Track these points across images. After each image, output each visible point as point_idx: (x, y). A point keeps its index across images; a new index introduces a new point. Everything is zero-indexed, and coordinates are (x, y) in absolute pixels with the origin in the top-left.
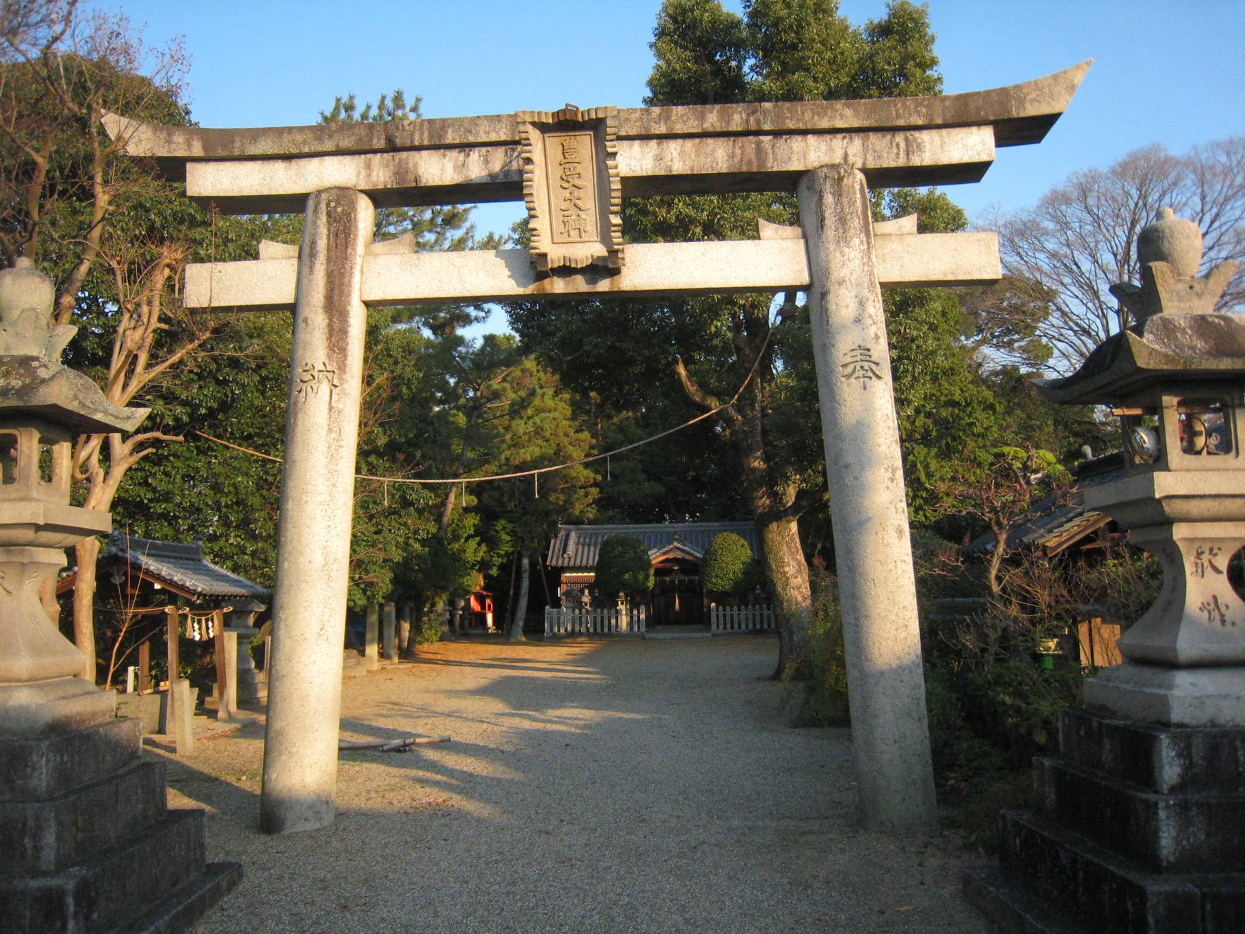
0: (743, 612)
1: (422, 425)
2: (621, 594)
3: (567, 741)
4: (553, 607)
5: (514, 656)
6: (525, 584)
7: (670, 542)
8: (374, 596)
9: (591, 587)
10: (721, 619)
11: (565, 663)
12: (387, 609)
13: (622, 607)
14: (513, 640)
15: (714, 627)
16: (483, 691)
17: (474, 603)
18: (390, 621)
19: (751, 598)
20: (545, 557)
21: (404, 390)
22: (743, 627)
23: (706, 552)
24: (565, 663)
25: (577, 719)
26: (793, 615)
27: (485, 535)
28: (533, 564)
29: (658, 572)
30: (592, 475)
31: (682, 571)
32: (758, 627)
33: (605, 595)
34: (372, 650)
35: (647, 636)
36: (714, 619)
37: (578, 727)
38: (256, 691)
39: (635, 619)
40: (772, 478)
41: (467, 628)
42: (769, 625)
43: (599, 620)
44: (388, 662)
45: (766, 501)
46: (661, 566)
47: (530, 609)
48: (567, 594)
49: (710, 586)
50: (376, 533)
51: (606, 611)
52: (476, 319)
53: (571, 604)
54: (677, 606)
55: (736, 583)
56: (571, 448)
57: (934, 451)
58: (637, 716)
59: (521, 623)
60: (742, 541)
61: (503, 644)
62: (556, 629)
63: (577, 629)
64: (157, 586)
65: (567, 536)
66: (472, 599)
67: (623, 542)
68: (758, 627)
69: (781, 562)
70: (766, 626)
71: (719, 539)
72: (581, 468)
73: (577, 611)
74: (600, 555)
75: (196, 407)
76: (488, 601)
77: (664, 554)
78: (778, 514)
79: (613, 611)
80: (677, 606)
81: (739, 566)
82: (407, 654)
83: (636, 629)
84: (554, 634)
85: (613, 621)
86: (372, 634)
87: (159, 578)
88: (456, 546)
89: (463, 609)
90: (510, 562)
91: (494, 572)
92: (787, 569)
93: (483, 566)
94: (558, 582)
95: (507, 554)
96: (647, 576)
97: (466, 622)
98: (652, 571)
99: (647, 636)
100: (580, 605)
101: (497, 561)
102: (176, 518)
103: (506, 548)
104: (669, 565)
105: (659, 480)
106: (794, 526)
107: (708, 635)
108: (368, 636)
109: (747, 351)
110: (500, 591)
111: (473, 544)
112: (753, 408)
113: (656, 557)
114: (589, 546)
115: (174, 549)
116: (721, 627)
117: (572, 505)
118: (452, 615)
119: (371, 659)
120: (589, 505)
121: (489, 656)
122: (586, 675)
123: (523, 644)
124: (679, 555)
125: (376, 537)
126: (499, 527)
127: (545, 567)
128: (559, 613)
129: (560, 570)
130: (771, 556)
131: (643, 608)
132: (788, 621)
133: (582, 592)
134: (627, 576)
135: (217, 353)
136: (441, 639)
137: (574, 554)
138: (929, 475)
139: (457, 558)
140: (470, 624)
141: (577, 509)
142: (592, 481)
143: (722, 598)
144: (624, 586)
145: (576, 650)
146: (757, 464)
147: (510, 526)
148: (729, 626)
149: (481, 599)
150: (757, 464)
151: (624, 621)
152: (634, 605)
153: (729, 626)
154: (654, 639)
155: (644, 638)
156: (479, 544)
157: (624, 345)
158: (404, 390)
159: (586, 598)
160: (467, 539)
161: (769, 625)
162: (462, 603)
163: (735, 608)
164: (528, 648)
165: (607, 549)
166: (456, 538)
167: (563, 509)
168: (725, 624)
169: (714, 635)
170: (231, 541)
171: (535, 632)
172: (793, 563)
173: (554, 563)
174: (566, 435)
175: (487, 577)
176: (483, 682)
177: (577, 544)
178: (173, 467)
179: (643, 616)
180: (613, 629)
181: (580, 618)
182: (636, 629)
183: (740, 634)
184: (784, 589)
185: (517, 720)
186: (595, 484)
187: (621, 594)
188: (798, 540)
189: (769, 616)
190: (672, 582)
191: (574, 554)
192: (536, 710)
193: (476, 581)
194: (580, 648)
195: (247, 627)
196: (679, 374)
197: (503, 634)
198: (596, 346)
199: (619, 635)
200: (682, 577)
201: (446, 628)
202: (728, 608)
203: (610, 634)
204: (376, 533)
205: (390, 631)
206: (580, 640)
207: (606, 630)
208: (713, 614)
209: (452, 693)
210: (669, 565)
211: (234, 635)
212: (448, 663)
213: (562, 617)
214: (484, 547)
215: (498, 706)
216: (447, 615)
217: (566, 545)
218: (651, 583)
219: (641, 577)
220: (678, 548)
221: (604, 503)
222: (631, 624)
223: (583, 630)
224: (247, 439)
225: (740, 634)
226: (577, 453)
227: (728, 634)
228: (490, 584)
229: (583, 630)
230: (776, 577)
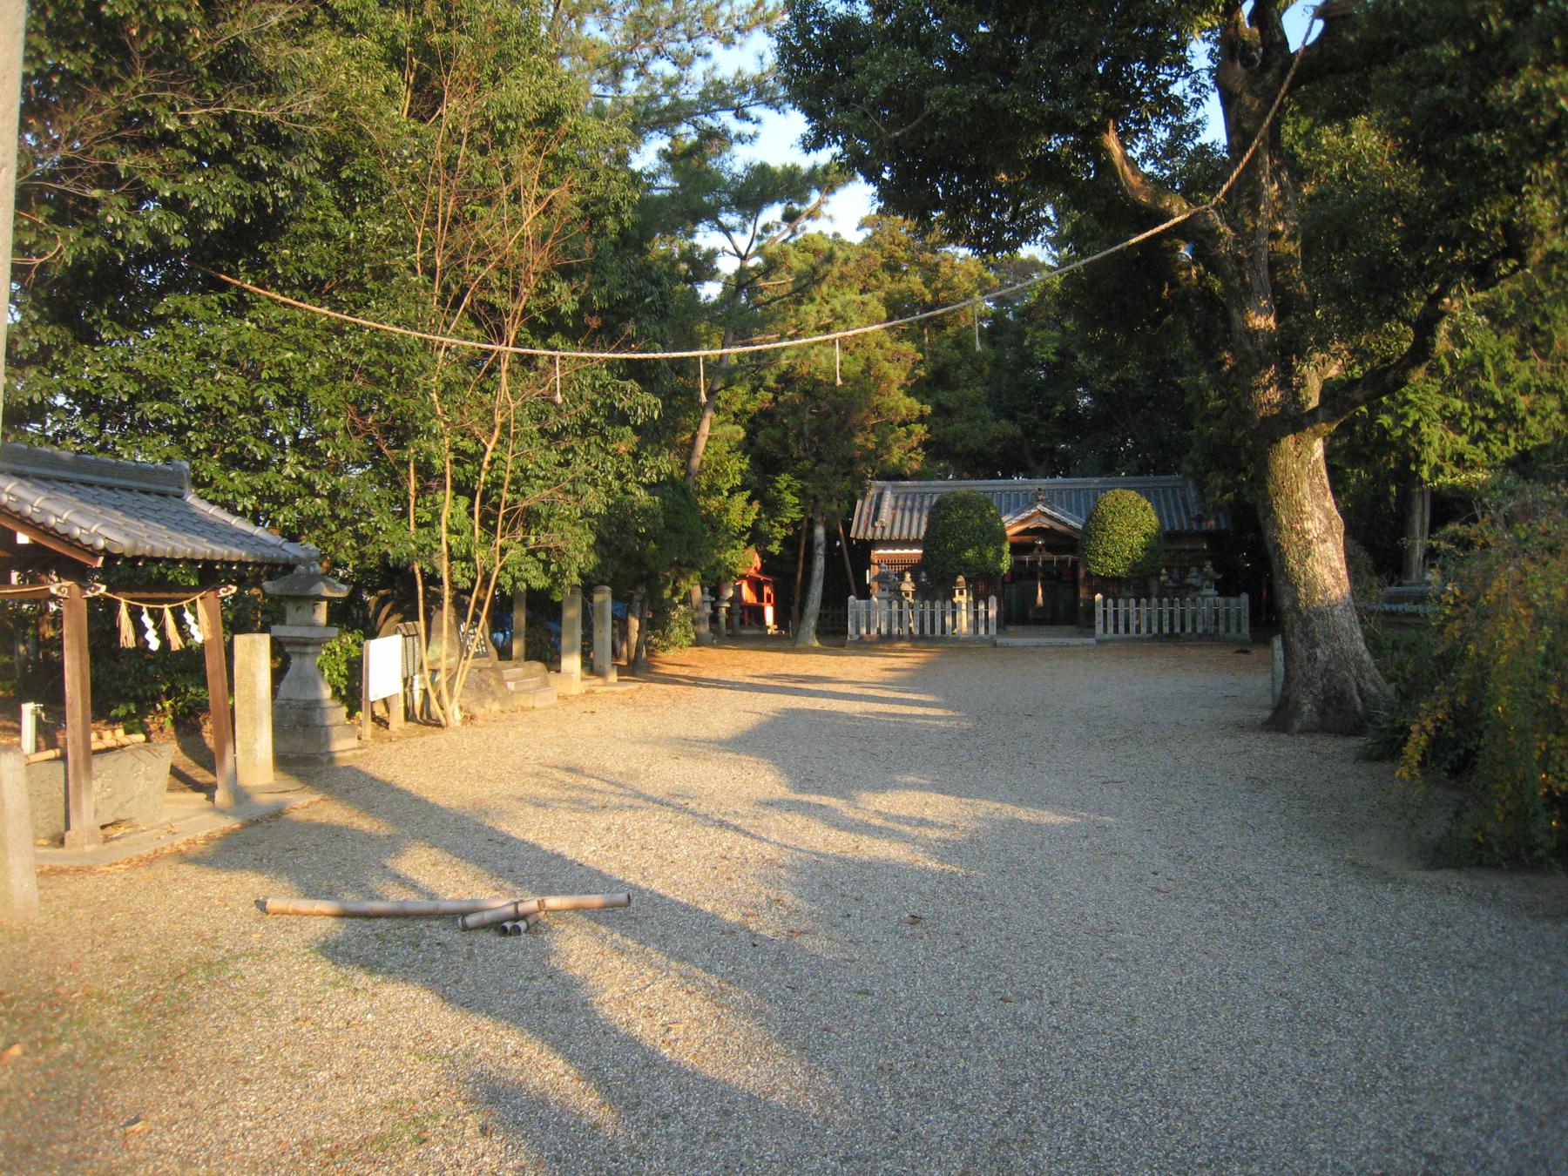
0: (1143, 609)
1: (641, 283)
2: (961, 579)
3: (913, 904)
4: (859, 598)
5: (801, 671)
6: (820, 564)
7: (1031, 505)
8: (562, 572)
9: (915, 569)
10: (1110, 618)
11: (884, 684)
12: (597, 598)
13: (962, 599)
14: (799, 646)
15: (1099, 629)
16: (743, 744)
17: (748, 595)
18: (441, 630)
19: (1154, 589)
20: (847, 527)
21: (610, 222)
22: (1144, 630)
23: (1089, 518)
24: (884, 684)
25: (922, 822)
26: (1320, 614)
27: (759, 489)
28: (831, 536)
29: (1016, 549)
30: (917, 406)
31: (1049, 547)
32: (1166, 630)
33: (935, 578)
34: (572, 663)
35: (1000, 641)
36: (1099, 618)
37: (928, 847)
38: (328, 740)
39: (982, 616)
40: (1286, 351)
41: (737, 627)
42: (1183, 629)
43: (927, 618)
44: (599, 681)
45: (1274, 395)
46: (1017, 539)
47: (825, 601)
48: (881, 579)
49: (1095, 569)
50: (560, 464)
51: (938, 604)
52: (739, 137)
53: (886, 594)
54: (1040, 599)
55: (1135, 564)
56: (887, 364)
57: (1511, 339)
58: (1048, 817)
59: (813, 623)
60: (1144, 502)
61: (786, 651)
62: (863, 631)
63: (895, 630)
64: (23, 539)
65: (880, 496)
66: (745, 586)
67: (964, 502)
68: (1166, 630)
69: (1299, 513)
70: (1177, 630)
71: (1109, 498)
72: (901, 394)
73: (895, 605)
74: (929, 524)
75: (198, 217)
76: (767, 590)
77: (1022, 522)
78: (1295, 420)
79: (949, 604)
80: (1040, 599)
81: (1138, 540)
82: (637, 668)
83: (982, 631)
84: (861, 638)
85: (949, 620)
86: (572, 634)
87: (27, 523)
88: (714, 503)
89: (730, 600)
90: (798, 534)
91: (775, 548)
92: (1308, 525)
93: (756, 537)
94: (868, 563)
95: (794, 524)
96: (1000, 553)
97: (736, 620)
98: (1007, 547)
99: (1000, 641)
100: (898, 593)
101: (780, 533)
102: (183, 429)
103: (793, 514)
104: (1027, 538)
105: (1011, 417)
106: (1318, 448)
107: (1091, 641)
108: (565, 642)
109: (1247, 99)
110: (783, 575)
111: (740, 500)
112: (1256, 214)
113: (1012, 525)
114: (911, 511)
115: (102, 469)
116: (1111, 629)
117: (888, 449)
118: (715, 609)
119: (569, 675)
120: (912, 449)
121: (763, 672)
122: (923, 709)
123: (816, 651)
124: (1046, 523)
125: (559, 471)
126: (781, 485)
127: (848, 540)
128: (868, 606)
129: (869, 545)
130: (1281, 500)
131: (993, 600)
132: (1307, 621)
133: (901, 576)
134: (970, 553)
135: (228, 109)
136: (698, 643)
137: (892, 520)
138: (1505, 379)
139: (714, 524)
140: (742, 622)
141: (896, 456)
142: (917, 413)
143: (1111, 585)
144: (965, 568)
145: (897, 662)
146: (1262, 321)
147: (797, 484)
148: (1121, 628)
149: (757, 587)
150: (1262, 321)
151: (964, 618)
152: (979, 597)
153: (1121, 628)
154: (1008, 646)
155: (995, 645)
156: (749, 501)
157: (1004, 98)
158: (610, 222)
159: (908, 586)
160: (732, 492)
161: (1183, 629)
162: (730, 593)
163: (1132, 601)
164: (823, 658)
165: (938, 514)
166: (713, 490)
167: (870, 456)
168: (1105, 626)
169: (1099, 642)
170: (287, 471)
171: (834, 633)
172: (1319, 514)
173: (861, 535)
174: (880, 345)
175: (765, 555)
176: (747, 721)
177: (895, 508)
178: (177, 337)
179: (992, 613)
180: (949, 631)
181: (900, 614)
182: (982, 631)
183: (1141, 640)
184: (1301, 562)
185: (799, 821)
186: (921, 419)
187: (961, 579)
188: (1324, 473)
189: (1227, 611)
190: (1034, 563)
191: (892, 520)
192: (839, 794)
193: (752, 561)
194: (905, 660)
195: (313, 625)
196: (1108, 151)
197: (786, 639)
198: (950, 101)
199: (956, 639)
200: (1048, 556)
201: (704, 629)
202: (1121, 602)
203: (944, 637)
204: (560, 464)
205: (604, 634)
206: (900, 645)
207: (938, 632)
208: (1099, 610)
209: (688, 746)
210: (1027, 538)
211: (263, 642)
212: (696, 682)
213: (871, 612)
214: (756, 506)
215: (765, 780)
216: (708, 610)
217: (878, 508)
218: (1006, 563)
219: (990, 554)
220: (1044, 514)
221: (935, 449)
222: (975, 624)
223: (905, 632)
224: (313, 288)
225: (1141, 640)
226: (897, 374)
227: (1122, 640)
228: (771, 565)
229: (905, 632)
230: (1288, 541)
